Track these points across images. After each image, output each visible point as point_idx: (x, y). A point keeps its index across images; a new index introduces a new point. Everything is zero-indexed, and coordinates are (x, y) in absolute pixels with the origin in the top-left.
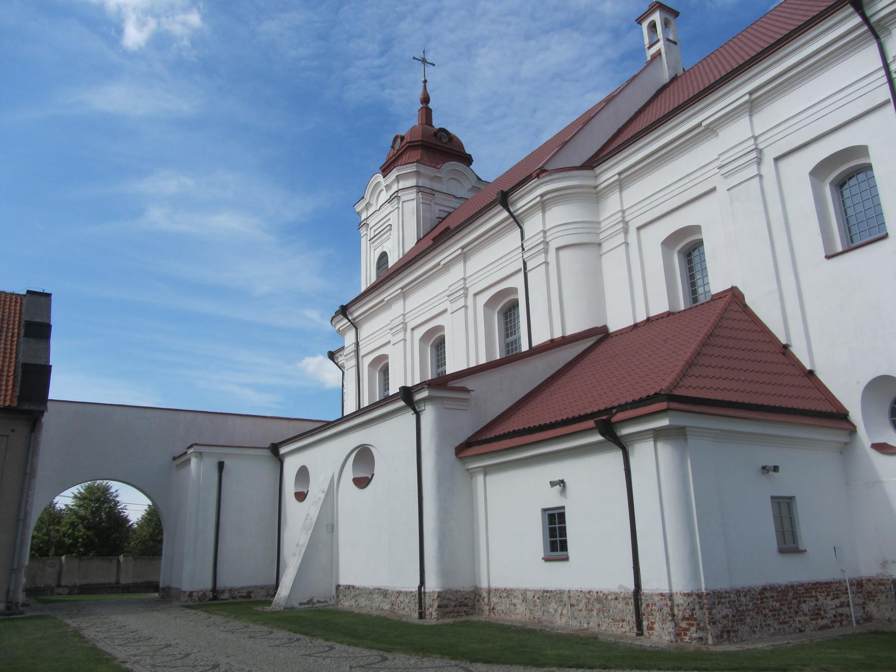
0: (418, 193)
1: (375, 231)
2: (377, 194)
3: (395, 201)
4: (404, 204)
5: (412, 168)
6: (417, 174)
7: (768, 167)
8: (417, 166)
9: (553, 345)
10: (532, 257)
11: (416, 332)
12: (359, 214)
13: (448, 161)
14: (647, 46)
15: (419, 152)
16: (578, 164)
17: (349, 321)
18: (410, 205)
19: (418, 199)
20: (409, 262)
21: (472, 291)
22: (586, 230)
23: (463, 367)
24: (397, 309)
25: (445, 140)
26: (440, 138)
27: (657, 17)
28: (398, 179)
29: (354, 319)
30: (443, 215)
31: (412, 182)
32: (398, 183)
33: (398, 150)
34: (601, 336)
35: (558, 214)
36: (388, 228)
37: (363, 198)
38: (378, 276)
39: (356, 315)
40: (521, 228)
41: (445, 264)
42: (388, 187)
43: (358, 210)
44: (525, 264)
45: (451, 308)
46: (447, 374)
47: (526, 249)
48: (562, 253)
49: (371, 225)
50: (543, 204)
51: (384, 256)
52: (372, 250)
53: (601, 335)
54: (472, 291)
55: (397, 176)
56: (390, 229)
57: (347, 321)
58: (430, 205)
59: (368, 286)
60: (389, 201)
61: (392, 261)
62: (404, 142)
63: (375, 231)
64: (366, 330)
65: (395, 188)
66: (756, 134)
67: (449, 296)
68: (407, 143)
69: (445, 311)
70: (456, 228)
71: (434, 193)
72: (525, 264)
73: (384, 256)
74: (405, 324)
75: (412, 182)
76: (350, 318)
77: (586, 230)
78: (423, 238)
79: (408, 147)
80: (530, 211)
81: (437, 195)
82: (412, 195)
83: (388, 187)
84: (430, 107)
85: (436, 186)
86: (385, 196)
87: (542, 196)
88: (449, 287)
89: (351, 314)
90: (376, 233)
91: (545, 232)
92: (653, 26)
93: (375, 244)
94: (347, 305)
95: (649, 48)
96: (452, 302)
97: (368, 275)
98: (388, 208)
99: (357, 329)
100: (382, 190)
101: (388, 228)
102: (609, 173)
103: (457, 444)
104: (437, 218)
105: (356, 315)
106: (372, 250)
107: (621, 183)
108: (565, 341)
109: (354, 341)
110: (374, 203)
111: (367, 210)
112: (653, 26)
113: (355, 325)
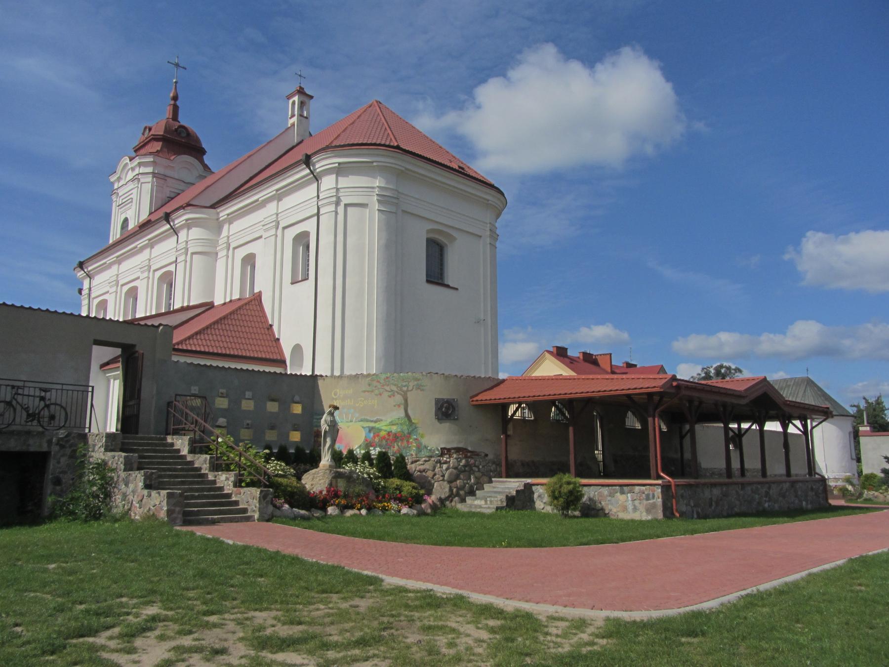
0: (153, 177)
1: (123, 199)
2: (125, 172)
3: (136, 182)
4: (143, 184)
5: (150, 159)
6: (154, 163)
7: (341, 209)
8: (154, 158)
9: (183, 309)
10: (324, 205)
11: (124, 287)
12: (113, 184)
13: (185, 153)
14: (290, 116)
15: (161, 143)
16: (208, 205)
17: (85, 272)
18: (147, 185)
19: (153, 182)
20: (145, 226)
21: (282, 225)
22: (201, 244)
23: (143, 315)
24: (114, 270)
25: (184, 135)
26: (180, 133)
27: (296, 98)
28: (140, 165)
29: (89, 272)
30: (173, 195)
31: (150, 169)
32: (140, 167)
33: (146, 138)
34: (208, 307)
35: (196, 233)
36: (130, 200)
37: (115, 172)
38: (121, 235)
39: (90, 269)
40: (177, 235)
41: (141, 247)
42: (133, 169)
43: (112, 180)
44: (176, 258)
45: (265, 235)
46: (137, 317)
47: (320, 198)
48: (194, 256)
49: (120, 195)
50: (188, 225)
51: (126, 221)
52: (120, 214)
53: (209, 306)
54: (282, 225)
55: (139, 163)
56: (132, 202)
57: (83, 272)
58: (162, 187)
59: (114, 239)
60: (132, 180)
61: (131, 225)
62: (152, 133)
63: (123, 199)
64: (98, 279)
65: (137, 172)
66: (339, 187)
67: (140, 268)
68: (152, 135)
69: (261, 237)
70: (154, 221)
71: (166, 178)
72: (176, 258)
73: (126, 221)
74: (118, 282)
75: (150, 169)
76: (86, 270)
77: (201, 244)
78: (155, 211)
79: (152, 139)
80: (182, 227)
81: (169, 179)
82: (149, 178)
83: (133, 169)
84: (178, 105)
85: (169, 172)
86: (130, 175)
87: (187, 220)
88: (265, 219)
89: (87, 268)
90: (124, 201)
91: (187, 242)
92: (294, 103)
93: (122, 209)
94: (84, 261)
95: (290, 118)
96: (266, 230)
97: (115, 234)
98: (131, 186)
99: (90, 278)
100: (129, 170)
101: (130, 200)
102: (224, 212)
103: (102, 363)
104: (168, 197)
105: (90, 269)
106: (120, 214)
107: (231, 220)
108: (189, 308)
109: (88, 287)
110: (124, 177)
111: (119, 182)
112: (294, 103)
113: (89, 276)
